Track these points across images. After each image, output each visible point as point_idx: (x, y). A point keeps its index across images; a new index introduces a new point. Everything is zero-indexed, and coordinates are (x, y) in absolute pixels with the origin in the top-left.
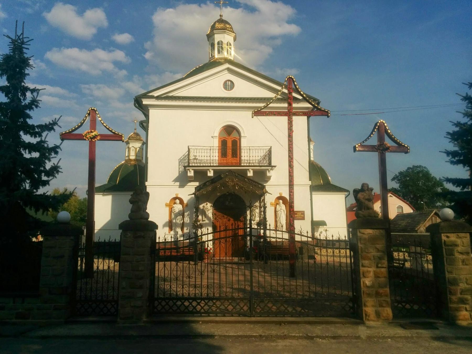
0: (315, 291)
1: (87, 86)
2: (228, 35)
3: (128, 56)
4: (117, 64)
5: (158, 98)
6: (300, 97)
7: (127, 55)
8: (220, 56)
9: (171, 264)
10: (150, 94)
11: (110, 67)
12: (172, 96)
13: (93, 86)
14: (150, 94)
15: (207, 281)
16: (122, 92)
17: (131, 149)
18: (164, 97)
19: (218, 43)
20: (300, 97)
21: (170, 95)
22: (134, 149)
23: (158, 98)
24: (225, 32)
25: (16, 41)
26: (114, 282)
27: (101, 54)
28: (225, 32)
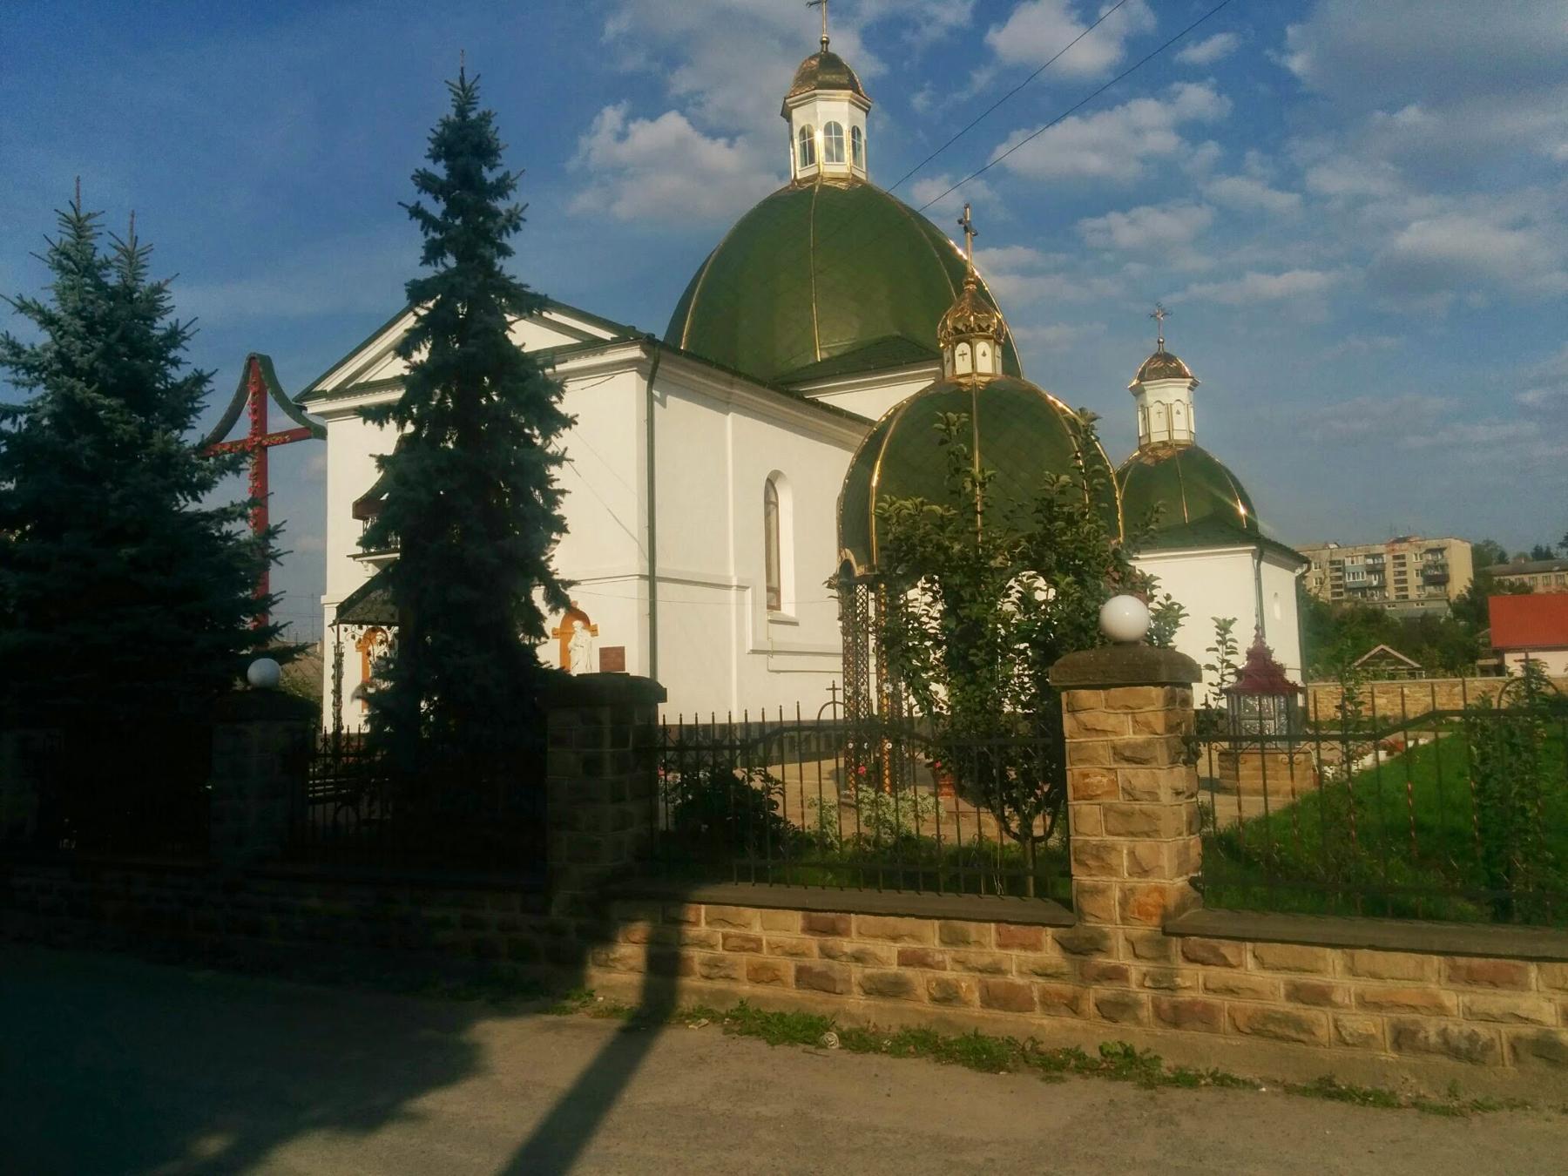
0: (957, 842)
1: (1099, 223)
2: (828, 100)
3: (1224, 97)
4: (1192, 131)
5: (339, 392)
6: (607, 335)
7: (1219, 90)
8: (810, 171)
9: (819, 767)
10: (319, 388)
11: (1163, 142)
12: (366, 382)
13: (1115, 219)
14: (319, 388)
15: (1262, 782)
16: (1202, 216)
17: (1153, 411)
18: (352, 387)
19: (803, 131)
20: (607, 335)
21: (362, 380)
22: (1162, 409)
23: (339, 392)
24: (815, 95)
25: (84, 309)
26: (802, 806)
27: (1147, 111)
28: (815, 95)
